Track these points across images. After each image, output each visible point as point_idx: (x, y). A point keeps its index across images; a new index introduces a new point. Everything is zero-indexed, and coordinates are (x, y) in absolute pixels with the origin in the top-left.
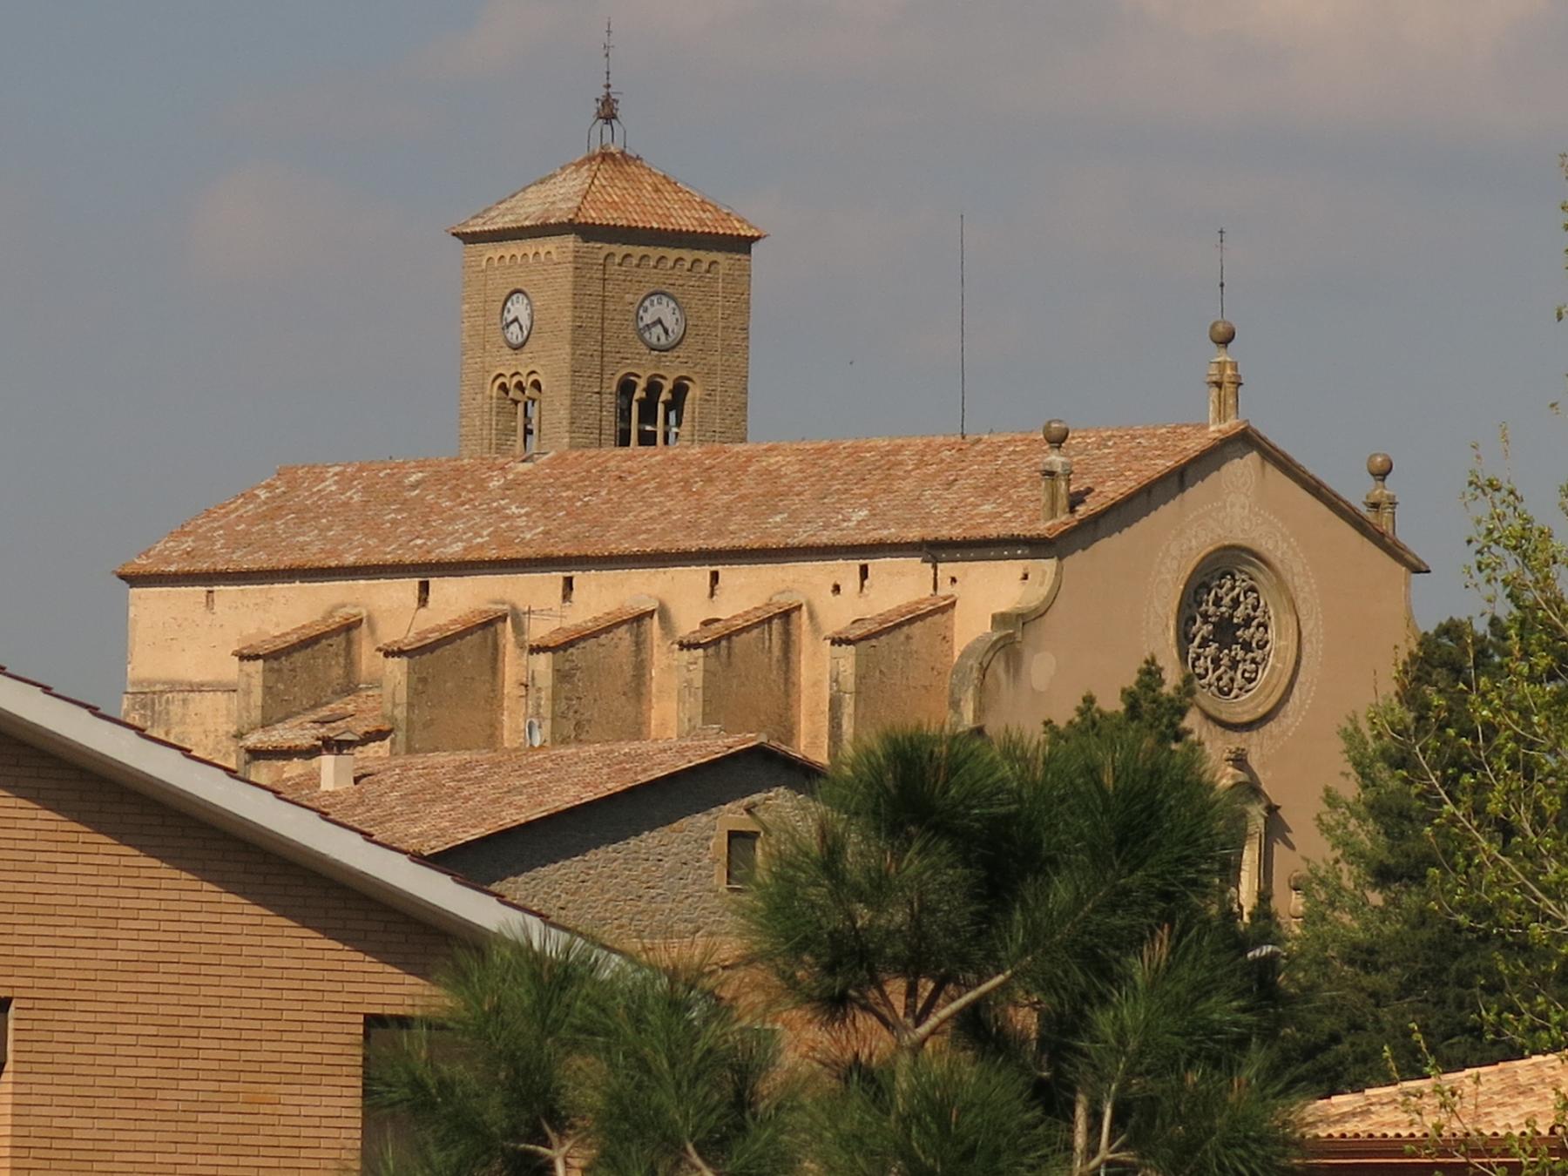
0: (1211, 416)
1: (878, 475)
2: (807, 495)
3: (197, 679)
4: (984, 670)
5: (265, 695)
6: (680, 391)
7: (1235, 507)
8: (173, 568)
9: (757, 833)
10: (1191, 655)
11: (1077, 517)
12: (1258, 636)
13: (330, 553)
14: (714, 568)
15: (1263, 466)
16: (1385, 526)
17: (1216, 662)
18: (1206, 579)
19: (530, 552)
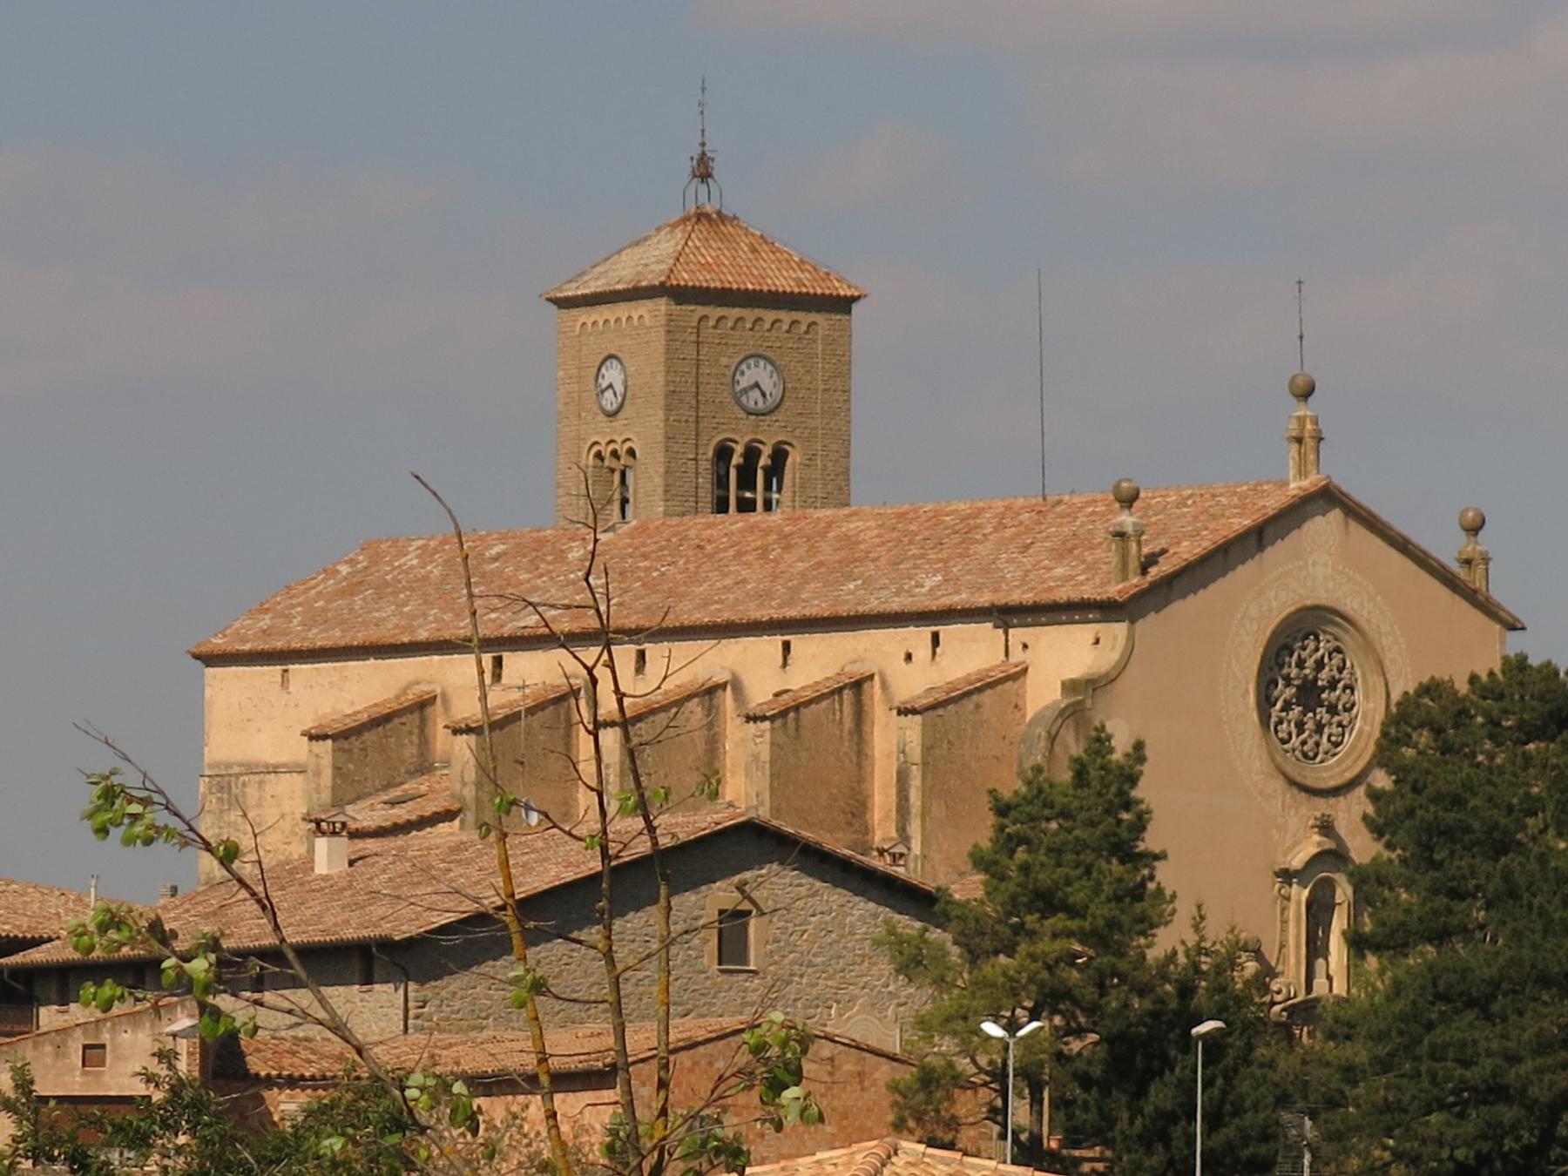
0: (1292, 473)
1: (956, 539)
2: (883, 561)
3: (273, 760)
4: (1052, 739)
6: (779, 456)
7: (1318, 564)
8: (247, 647)
9: (750, 912)
10: (1274, 719)
11: (1149, 578)
12: (1344, 698)
14: (786, 638)
15: (1347, 523)
16: (1479, 584)
17: (1300, 726)
18: (1289, 640)
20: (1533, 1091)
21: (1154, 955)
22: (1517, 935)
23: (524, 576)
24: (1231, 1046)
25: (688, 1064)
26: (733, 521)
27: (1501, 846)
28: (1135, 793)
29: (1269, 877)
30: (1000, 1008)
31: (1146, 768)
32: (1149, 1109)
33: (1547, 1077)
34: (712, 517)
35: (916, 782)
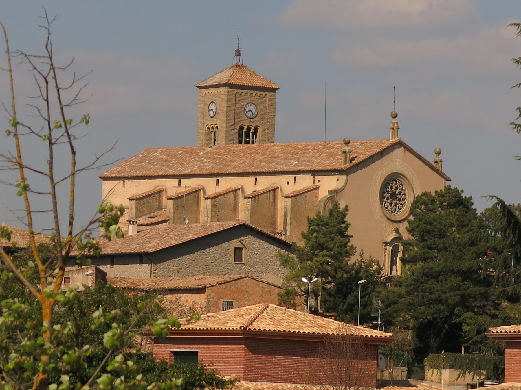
0: (391, 137)
1: (301, 152)
4: (325, 205)
5: (136, 210)
6: (256, 129)
7: (397, 162)
8: (114, 175)
10: (384, 202)
12: (403, 197)
13: (157, 172)
16: (439, 168)
17: (391, 204)
19: (207, 172)
20: (449, 301)
21: (350, 263)
22: (446, 260)
23: (188, 159)
24: (369, 287)
25: (224, 287)
26: (243, 146)
27: (442, 236)
28: (346, 219)
29: (381, 244)
30: (308, 274)
31: (348, 213)
32: (347, 303)
33: (453, 298)
34: (238, 145)
35: (289, 216)
